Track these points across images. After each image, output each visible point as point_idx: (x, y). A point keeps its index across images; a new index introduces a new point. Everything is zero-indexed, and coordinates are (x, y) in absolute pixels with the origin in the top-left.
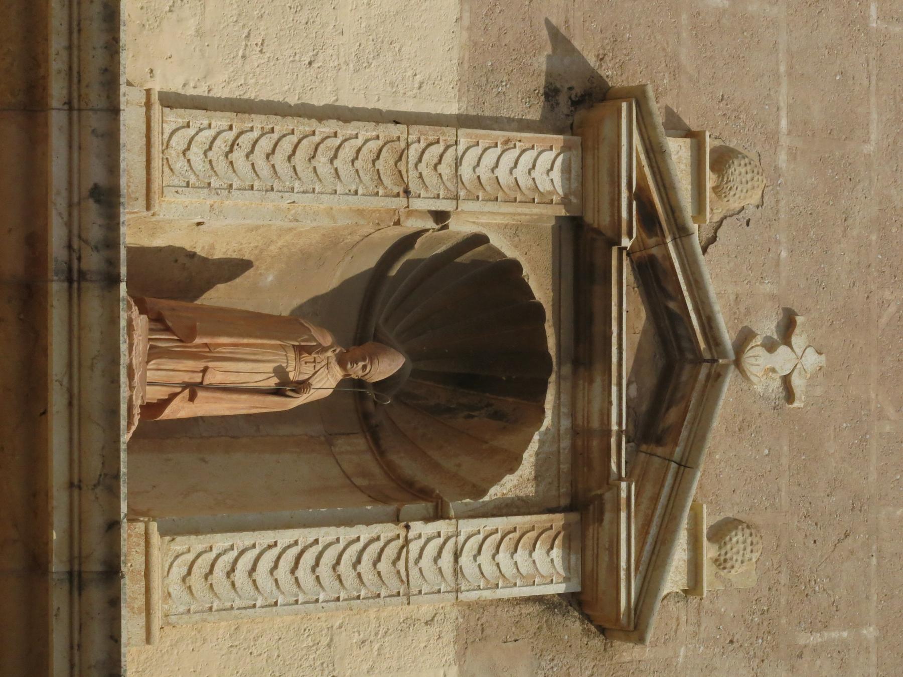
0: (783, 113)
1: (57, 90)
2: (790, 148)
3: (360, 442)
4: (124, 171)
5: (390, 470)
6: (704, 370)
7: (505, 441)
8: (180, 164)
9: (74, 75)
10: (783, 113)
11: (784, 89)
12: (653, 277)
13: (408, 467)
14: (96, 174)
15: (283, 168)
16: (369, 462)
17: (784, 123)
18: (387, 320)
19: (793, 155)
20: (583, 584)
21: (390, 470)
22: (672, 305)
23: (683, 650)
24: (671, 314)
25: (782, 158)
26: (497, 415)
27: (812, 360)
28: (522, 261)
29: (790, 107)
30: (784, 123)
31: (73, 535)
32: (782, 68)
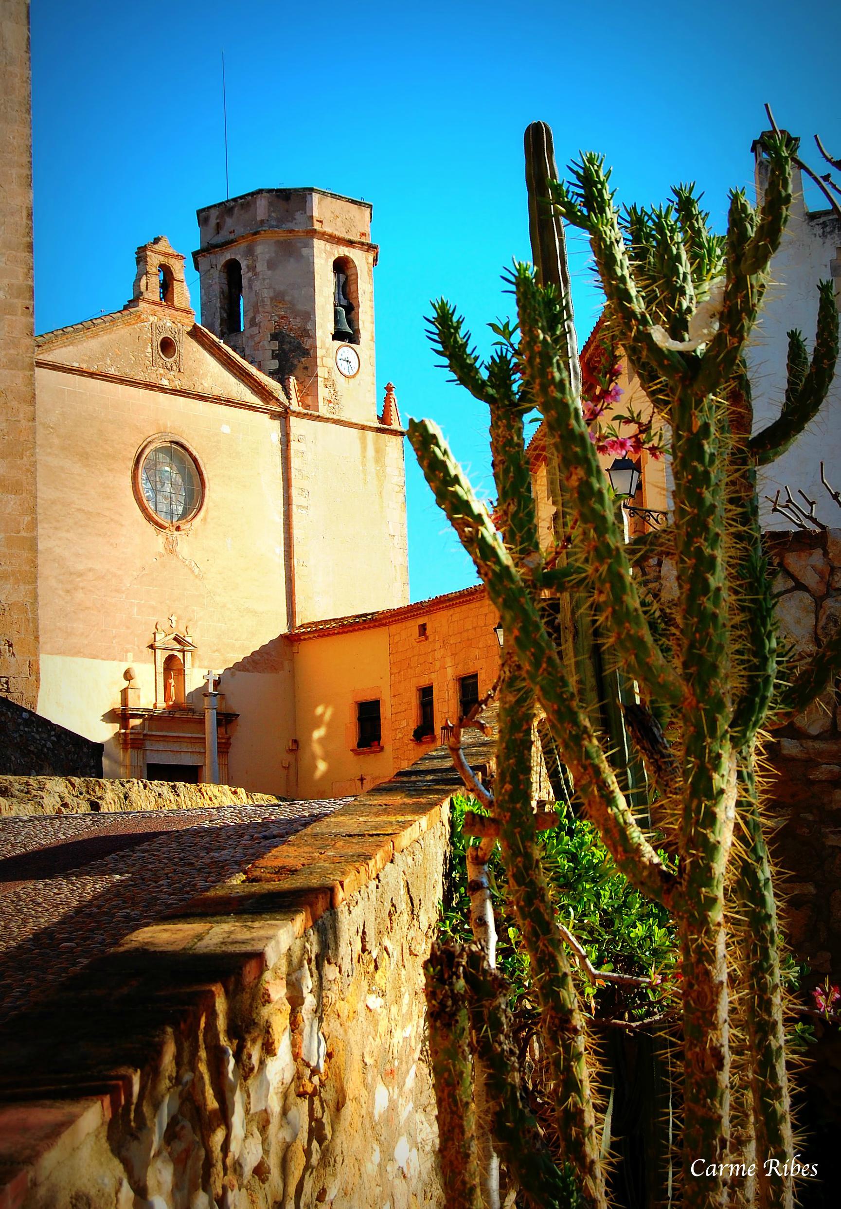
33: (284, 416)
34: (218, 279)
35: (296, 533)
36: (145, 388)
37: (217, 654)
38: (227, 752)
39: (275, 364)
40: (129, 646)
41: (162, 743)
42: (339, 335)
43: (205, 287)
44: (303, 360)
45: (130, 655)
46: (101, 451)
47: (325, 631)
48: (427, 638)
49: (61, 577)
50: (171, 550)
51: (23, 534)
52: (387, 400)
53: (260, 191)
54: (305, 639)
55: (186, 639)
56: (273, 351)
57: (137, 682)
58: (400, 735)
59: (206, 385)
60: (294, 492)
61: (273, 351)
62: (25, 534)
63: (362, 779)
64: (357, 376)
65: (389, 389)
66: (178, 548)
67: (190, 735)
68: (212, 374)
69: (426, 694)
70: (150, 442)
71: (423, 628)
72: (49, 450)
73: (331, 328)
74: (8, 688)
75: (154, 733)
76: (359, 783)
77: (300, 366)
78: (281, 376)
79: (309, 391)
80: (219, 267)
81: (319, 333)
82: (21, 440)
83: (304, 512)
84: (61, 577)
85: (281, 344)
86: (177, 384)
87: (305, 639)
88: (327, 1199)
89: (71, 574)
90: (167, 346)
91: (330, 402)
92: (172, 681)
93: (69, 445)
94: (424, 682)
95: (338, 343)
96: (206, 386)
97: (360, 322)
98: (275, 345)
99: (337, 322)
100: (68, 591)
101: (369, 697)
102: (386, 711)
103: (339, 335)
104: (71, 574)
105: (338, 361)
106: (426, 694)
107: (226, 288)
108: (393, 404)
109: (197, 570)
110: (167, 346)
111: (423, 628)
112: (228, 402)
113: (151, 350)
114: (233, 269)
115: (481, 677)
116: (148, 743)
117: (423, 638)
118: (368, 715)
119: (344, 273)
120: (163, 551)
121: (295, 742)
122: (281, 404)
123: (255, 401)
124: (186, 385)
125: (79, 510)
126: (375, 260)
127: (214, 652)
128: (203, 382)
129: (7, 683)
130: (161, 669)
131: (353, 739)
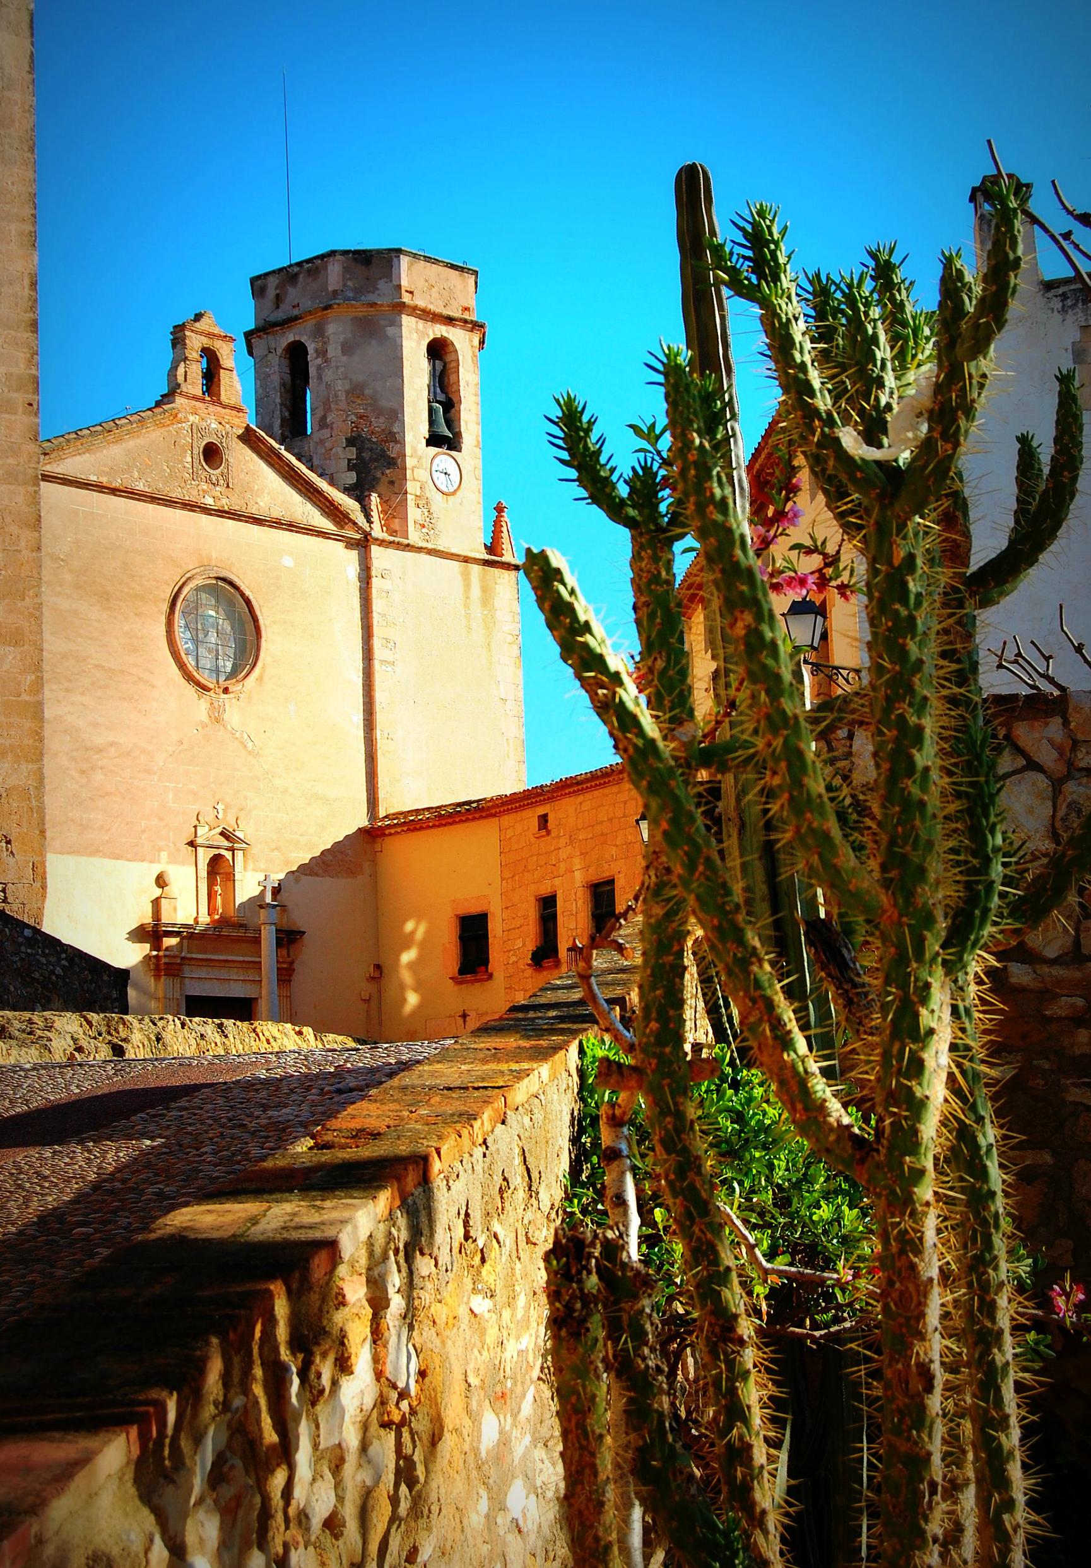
33: (363, 544)
34: (277, 367)
35: (379, 696)
36: (183, 509)
37: (276, 853)
38: (290, 981)
39: (351, 478)
40: (162, 843)
41: (205, 969)
42: (434, 440)
43: (261, 378)
44: (388, 471)
45: (164, 855)
46: (126, 590)
47: (417, 823)
48: (549, 833)
49: (74, 754)
50: (217, 718)
51: (25, 697)
52: (497, 524)
53: (333, 253)
54: (390, 834)
55: (237, 833)
56: (349, 460)
57: (173, 889)
58: (514, 959)
59: (261, 504)
60: (377, 643)
61: (349, 460)
62: (27, 698)
63: (464, 1016)
64: (458, 493)
65: (500, 509)
66: (226, 717)
67: (241, 959)
68: (269, 490)
69: (548, 905)
70: (189, 578)
71: (544, 820)
72: (58, 589)
73: (424, 431)
74: (5, 897)
75: (194, 956)
76: (460, 1020)
77: (384, 480)
78: (359, 492)
79: (395, 512)
80: (279, 351)
81: (409, 437)
82: (23, 575)
83: (389, 669)
84: (74, 754)
85: (360, 451)
86: (225, 503)
87: (390, 834)
88: (419, 1560)
89: (87, 749)
90: (212, 454)
91: (424, 526)
92: (218, 888)
93: (85, 582)
94: (545, 890)
95: (433, 450)
96: (262, 506)
97: (462, 423)
98: (352, 453)
99: (432, 422)
100: (83, 772)
101: (474, 909)
102: (495, 928)
103: (434, 440)
104: (87, 749)
105: (434, 473)
106: (548, 905)
107: (288, 378)
108: (504, 529)
109: (250, 744)
110: (212, 454)
111: (544, 820)
112: (291, 527)
113: (190, 459)
114: (297, 354)
115: (619, 883)
116: (186, 969)
117: (543, 832)
118: (473, 932)
119: (441, 359)
120: (206, 719)
121: (378, 967)
122: (359, 529)
123: (327, 525)
124: (236, 504)
125: (97, 666)
126: (482, 342)
127: (273, 850)
128: (259, 500)
129: (4, 891)
130: (203, 873)
131: (453, 964)
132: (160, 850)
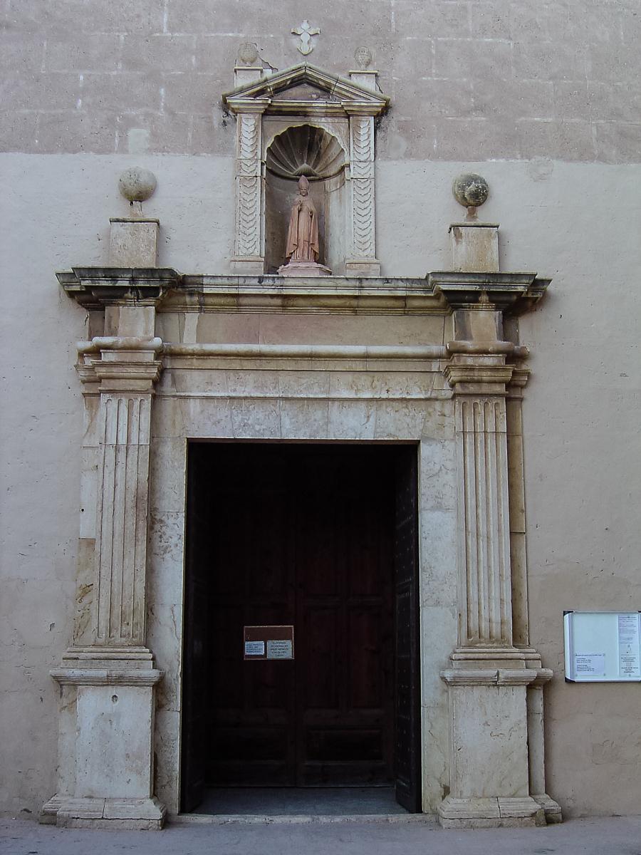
0: (227, 35)
1: (233, 291)
2: (239, 32)
3: (327, 182)
4: (310, 436)
5: (335, 175)
6: (307, 71)
7: (329, 139)
8: (251, 250)
9: (231, 286)
10: (227, 35)
11: (220, 34)
12: (279, 89)
13: (334, 169)
14: (255, 281)
15: (251, 218)
16: (333, 180)
17: (230, 35)
18: (291, 171)
19: (240, 31)
20: (371, 116)
21: (335, 175)
22: (288, 83)
23: (394, 78)
24: (291, 83)
25: (241, 35)
26: (320, 140)
27: (305, 26)
28: (274, 136)
29: (225, 32)
30: (230, 35)
31: (346, 288)
32: (213, 35)
41: (251, 377)
45: (139, 136)
67: (359, 349)
132: (130, 123)
